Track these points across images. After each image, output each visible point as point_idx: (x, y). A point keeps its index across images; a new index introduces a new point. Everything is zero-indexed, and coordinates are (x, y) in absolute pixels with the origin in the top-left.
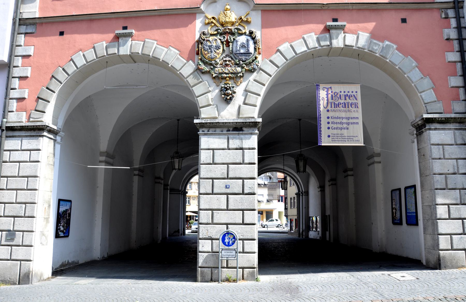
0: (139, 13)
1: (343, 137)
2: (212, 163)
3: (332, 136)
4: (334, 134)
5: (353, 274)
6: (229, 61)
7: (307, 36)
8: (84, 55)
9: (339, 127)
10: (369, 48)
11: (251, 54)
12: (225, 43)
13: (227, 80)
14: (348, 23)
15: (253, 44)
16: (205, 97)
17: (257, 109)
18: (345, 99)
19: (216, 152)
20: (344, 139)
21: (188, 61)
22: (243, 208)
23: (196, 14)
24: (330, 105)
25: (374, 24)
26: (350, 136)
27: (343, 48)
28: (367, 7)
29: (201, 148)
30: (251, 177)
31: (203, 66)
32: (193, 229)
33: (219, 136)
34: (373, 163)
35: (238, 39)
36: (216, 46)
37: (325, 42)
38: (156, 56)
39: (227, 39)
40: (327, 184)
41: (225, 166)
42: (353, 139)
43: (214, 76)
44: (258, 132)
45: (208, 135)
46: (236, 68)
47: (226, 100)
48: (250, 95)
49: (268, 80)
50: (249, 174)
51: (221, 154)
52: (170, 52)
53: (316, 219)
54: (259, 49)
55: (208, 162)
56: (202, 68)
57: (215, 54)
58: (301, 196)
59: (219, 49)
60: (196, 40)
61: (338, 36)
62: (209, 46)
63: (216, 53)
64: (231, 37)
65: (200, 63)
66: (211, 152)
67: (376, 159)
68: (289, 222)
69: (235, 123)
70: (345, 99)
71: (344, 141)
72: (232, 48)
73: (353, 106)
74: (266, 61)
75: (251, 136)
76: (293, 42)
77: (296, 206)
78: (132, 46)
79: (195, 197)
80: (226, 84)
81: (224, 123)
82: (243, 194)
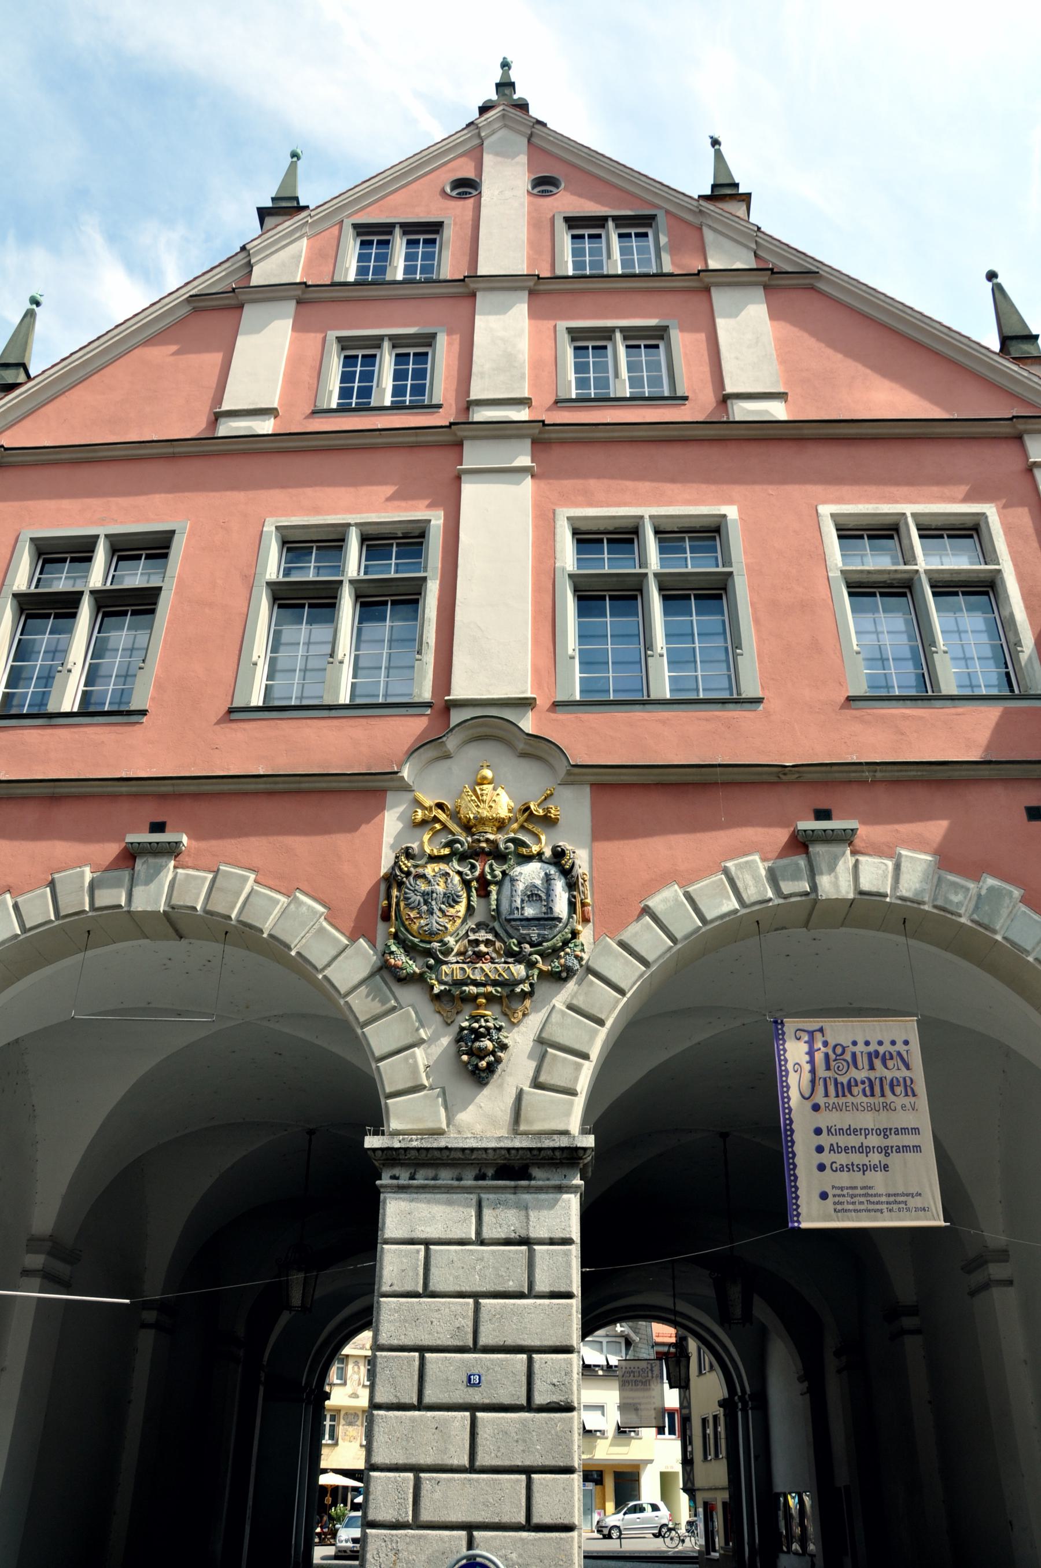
0: (206, 784)
1: (872, 1199)
2: (420, 1290)
3: (834, 1196)
4: (842, 1188)
6: (487, 943)
7: (736, 865)
8: (16, 906)
9: (855, 1163)
10: (935, 899)
11: (560, 922)
12: (474, 884)
13: (478, 1007)
14: (863, 822)
15: (566, 888)
16: (406, 1059)
17: (579, 1104)
18: (872, 1067)
19: (436, 1251)
20: (878, 1203)
21: (353, 938)
22: (527, 1463)
23: (384, 791)
24: (820, 1089)
26: (895, 1195)
27: (853, 900)
28: (919, 773)
29: (386, 1236)
30: (558, 1344)
31: (401, 959)
32: (344, 1544)
33: (448, 1196)
34: (986, 1286)
35: (517, 873)
36: (445, 894)
37: (796, 883)
38: (250, 921)
39: (483, 874)
40: (831, 1363)
41: (468, 1304)
42: (905, 1203)
43: (436, 991)
44: (582, 1182)
45: (411, 1193)
46: (511, 966)
47: (473, 1073)
48: (555, 1055)
49: (615, 1008)
50: (552, 1332)
51: (455, 1259)
52: (297, 908)
53: (801, 1502)
54: (583, 905)
55: (409, 1287)
57: (443, 921)
58: (740, 1413)
59: (457, 903)
60: (382, 874)
61: (836, 865)
62: (424, 894)
63: (446, 915)
64: (495, 866)
65: (394, 948)
66: (418, 1251)
67: (996, 1271)
68: (702, 1516)
69: (503, 1152)
70: (872, 1067)
71: (876, 1211)
72: (497, 900)
73: (898, 1090)
74: (607, 942)
75: (558, 1196)
76: (692, 882)
77: (723, 1454)
78: (176, 885)
79: (356, 1415)
80: (475, 1018)
81: (467, 1152)
82: (529, 1407)
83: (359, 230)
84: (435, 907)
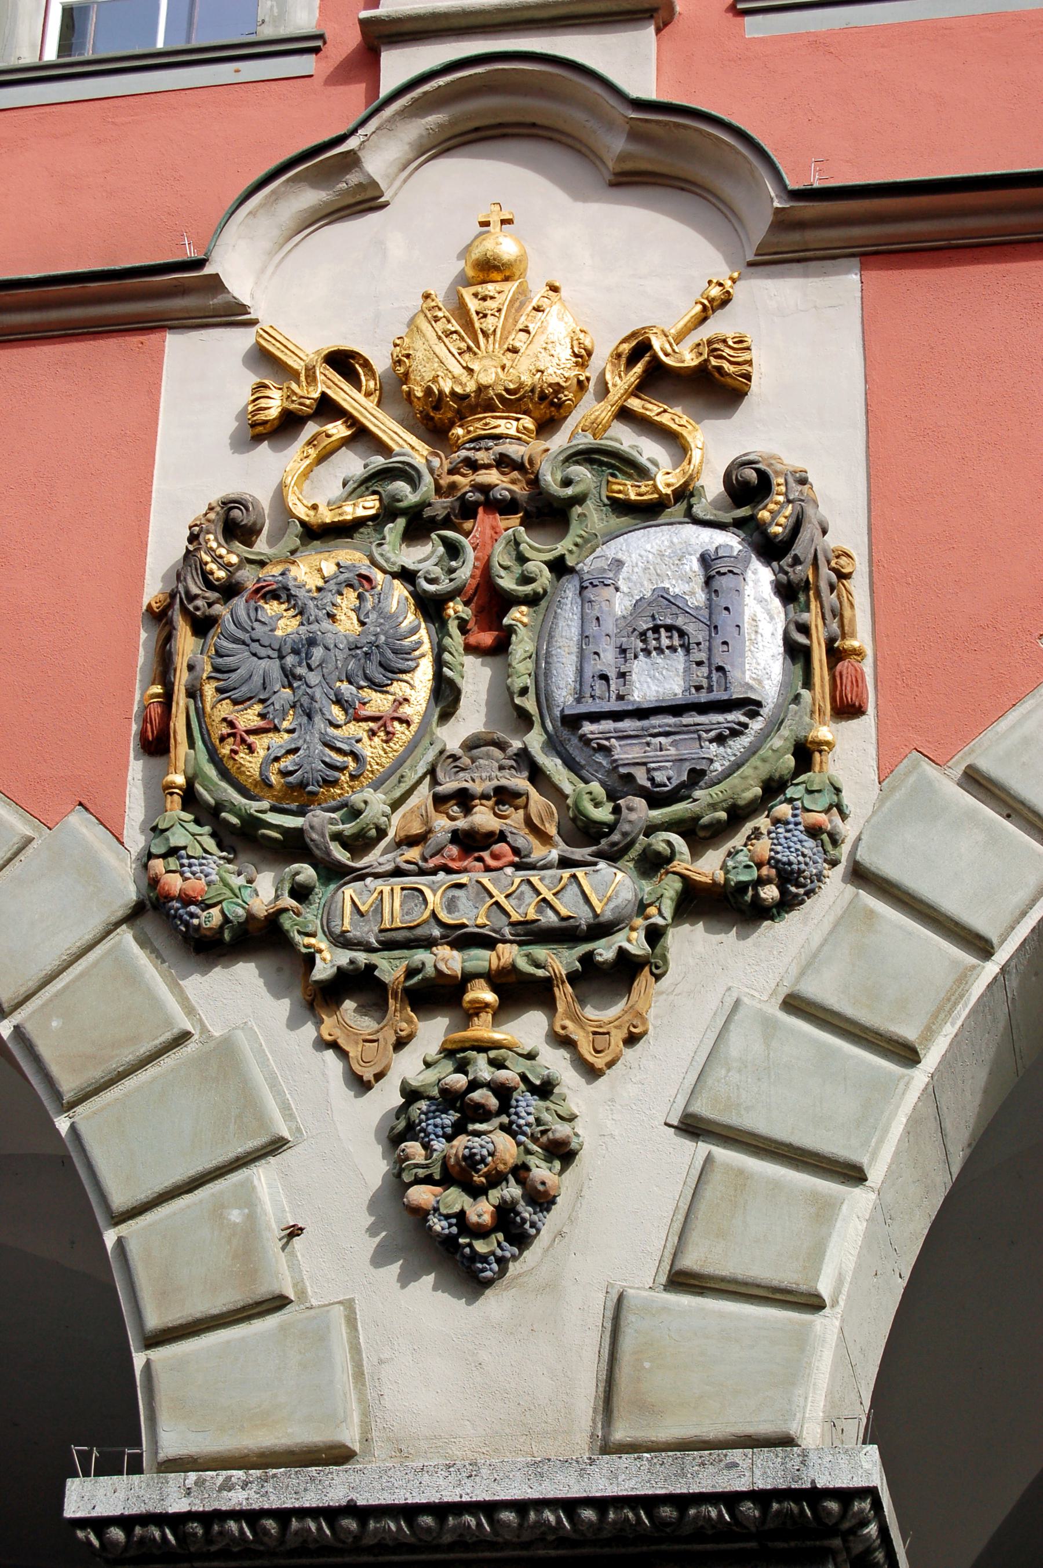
5: (948, 1037)
16: (218, 1211)
25: (459, 1115)
43: (322, 971)
46: (580, 872)
48: (741, 1173)
54: (835, 655)
56: (196, 886)
59: (394, 672)
83: (219, 300)
84: (318, 694)
